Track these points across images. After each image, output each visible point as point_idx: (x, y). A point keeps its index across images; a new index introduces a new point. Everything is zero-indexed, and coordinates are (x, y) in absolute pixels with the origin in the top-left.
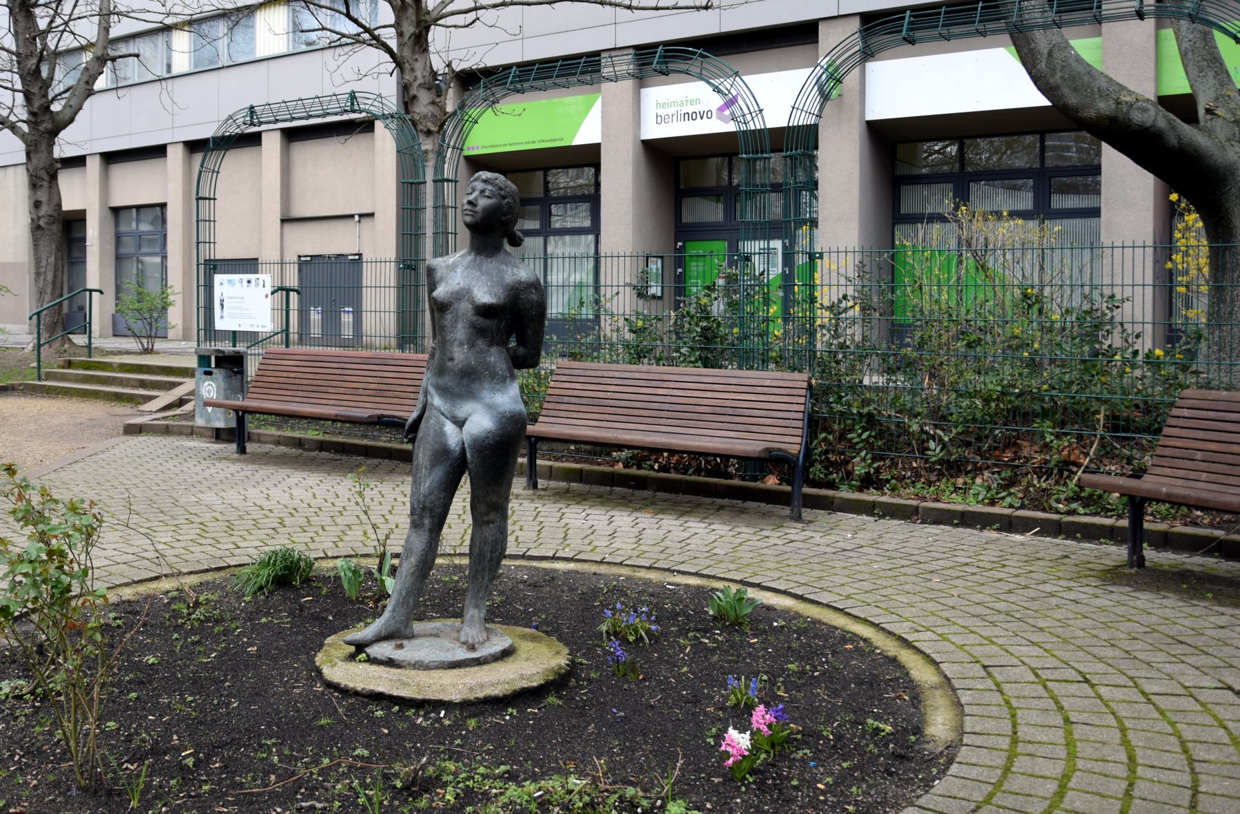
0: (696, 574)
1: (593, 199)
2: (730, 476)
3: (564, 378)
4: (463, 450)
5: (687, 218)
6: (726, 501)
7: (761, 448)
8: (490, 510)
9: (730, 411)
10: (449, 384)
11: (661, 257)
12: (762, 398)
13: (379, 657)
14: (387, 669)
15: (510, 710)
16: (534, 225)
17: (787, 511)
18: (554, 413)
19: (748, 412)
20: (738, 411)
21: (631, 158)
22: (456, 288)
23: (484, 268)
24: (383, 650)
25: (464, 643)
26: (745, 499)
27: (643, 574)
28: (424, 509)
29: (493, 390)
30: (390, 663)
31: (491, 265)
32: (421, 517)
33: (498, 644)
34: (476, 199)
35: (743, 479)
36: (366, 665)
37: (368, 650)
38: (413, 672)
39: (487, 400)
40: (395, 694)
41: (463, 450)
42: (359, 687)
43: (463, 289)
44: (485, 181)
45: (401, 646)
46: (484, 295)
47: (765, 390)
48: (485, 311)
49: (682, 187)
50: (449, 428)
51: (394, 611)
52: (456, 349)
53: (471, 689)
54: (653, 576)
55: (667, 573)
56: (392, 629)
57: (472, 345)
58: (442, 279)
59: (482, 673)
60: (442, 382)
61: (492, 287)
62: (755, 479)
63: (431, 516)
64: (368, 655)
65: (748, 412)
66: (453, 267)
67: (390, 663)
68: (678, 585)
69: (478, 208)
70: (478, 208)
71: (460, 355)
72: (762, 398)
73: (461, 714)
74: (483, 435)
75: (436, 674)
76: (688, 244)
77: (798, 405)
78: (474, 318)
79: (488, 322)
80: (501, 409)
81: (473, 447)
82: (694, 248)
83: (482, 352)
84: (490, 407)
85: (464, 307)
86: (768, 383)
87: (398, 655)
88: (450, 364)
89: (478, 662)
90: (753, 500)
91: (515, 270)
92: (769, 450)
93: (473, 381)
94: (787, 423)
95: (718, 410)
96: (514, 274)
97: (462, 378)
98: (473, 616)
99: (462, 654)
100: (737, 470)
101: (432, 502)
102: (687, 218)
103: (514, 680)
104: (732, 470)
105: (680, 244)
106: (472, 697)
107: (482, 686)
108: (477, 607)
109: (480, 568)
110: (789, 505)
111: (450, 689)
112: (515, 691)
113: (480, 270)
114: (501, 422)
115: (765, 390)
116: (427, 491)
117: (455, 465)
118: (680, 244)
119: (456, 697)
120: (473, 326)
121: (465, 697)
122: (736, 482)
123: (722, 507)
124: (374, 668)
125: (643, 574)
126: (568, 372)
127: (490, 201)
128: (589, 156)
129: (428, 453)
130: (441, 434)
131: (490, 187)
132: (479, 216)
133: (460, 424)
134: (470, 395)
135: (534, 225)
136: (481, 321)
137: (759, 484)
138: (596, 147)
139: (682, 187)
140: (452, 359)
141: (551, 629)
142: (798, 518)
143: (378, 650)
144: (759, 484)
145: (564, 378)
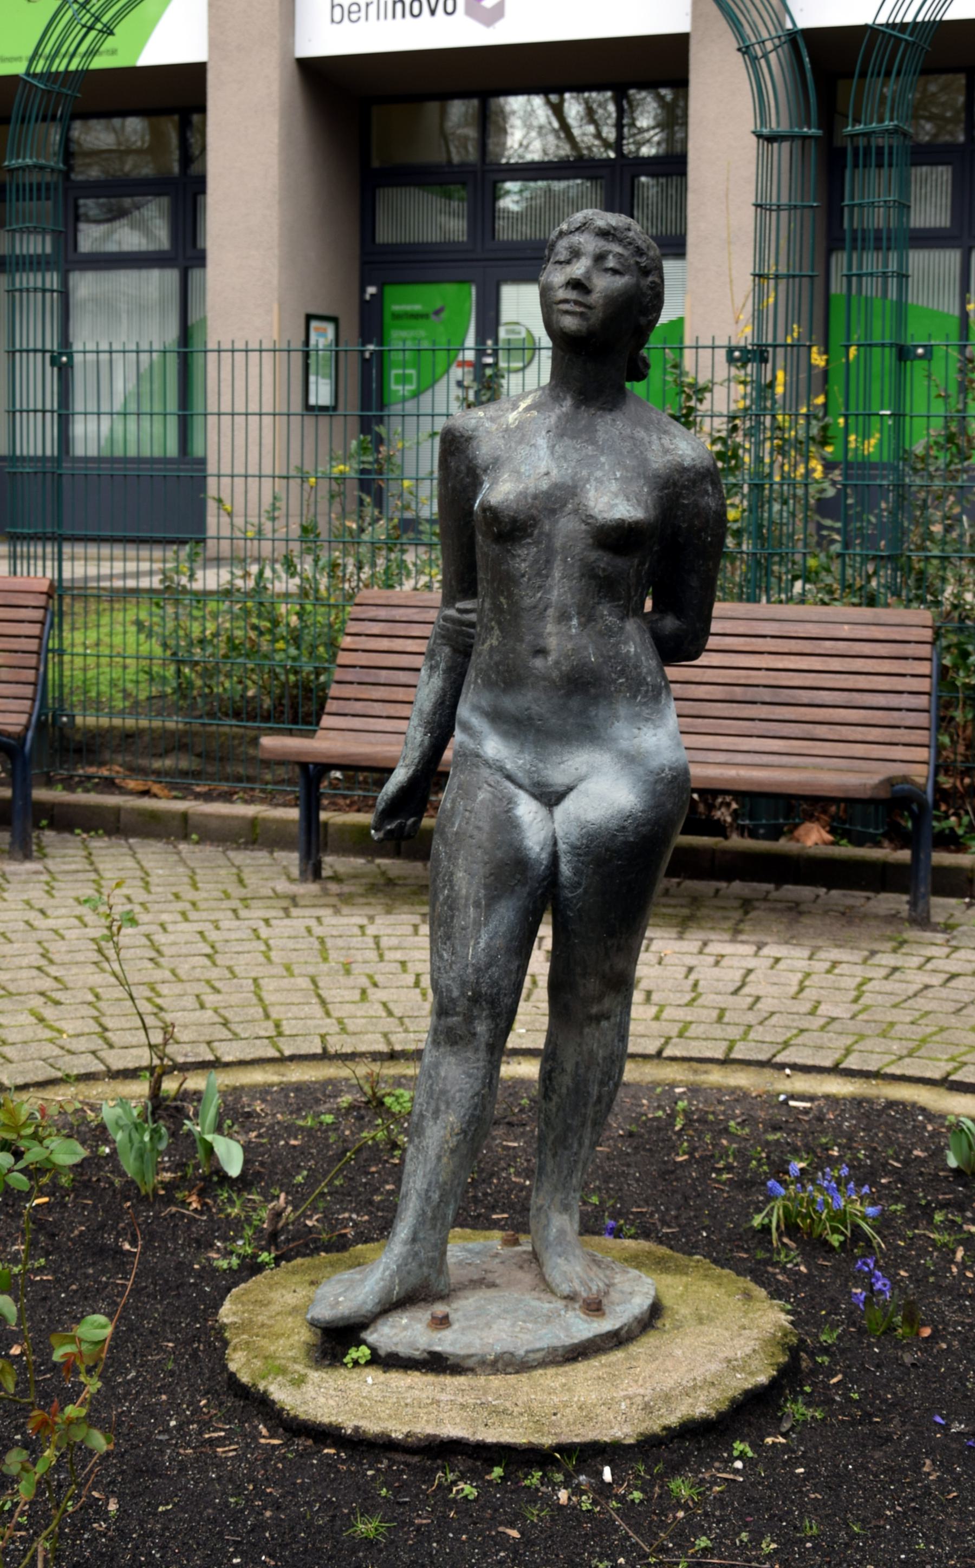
0: (836, 1070)
1: (184, 191)
2: (719, 829)
3: (376, 628)
4: (555, 857)
5: (385, 234)
6: (805, 892)
7: (875, 779)
8: (594, 985)
9: (767, 695)
10: (535, 708)
11: (334, 320)
12: (835, 664)
13: (403, 1351)
14: (430, 1378)
15: (739, 1446)
16: (37, 245)
17: (897, 902)
18: (358, 707)
19: (805, 696)
20: (785, 695)
21: (277, 106)
22: (544, 485)
23: (601, 436)
24: (405, 1332)
25: (571, 1298)
26: (780, 881)
27: (715, 1077)
28: (475, 1000)
29: (637, 719)
30: (435, 1363)
31: (611, 427)
32: (469, 1019)
33: (634, 1293)
34: (588, 274)
35: (753, 834)
36: (372, 1376)
37: (371, 1336)
38: (496, 1381)
39: (624, 744)
40: (490, 1439)
41: (555, 857)
42: (398, 1431)
43: (556, 486)
44: (605, 234)
45: (443, 1322)
46: (614, 501)
47: (842, 647)
48: (615, 538)
49: (376, 164)
50: (527, 809)
51: (414, 1239)
52: (550, 628)
53: (647, 1408)
54: (741, 1079)
55: (768, 1073)
56: (413, 1281)
57: (588, 617)
58: (496, 464)
59: (644, 1368)
60: (509, 703)
61: (625, 480)
62: (775, 833)
63: (473, 1011)
64: (374, 1350)
65: (805, 696)
66: (519, 434)
67: (435, 1363)
68: (811, 1098)
69: (595, 298)
70: (595, 298)
71: (560, 640)
72: (835, 664)
73: (649, 1470)
74: (613, 824)
75: (551, 1378)
76: (390, 291)
77: (918, 679)
78: (593, 555)
79: (620, 562)
80: (655, 763)
81: (575, 850)
82: (403, 300)
83: (609, 632)
84: (631, 759)
85: (566, 528)
86: (846, 631)
87: (447, 1342)
88: (538, 663)
89: (617, 1340)
90: (796, 883)
91: (666, 441)
92: (890, 782)
93: (595, 700)
94: (893, 718)
95: (738, 693)
96: (666, 451)
97: (569, 695)
98: (562, 1232)
99: (584, 1328)
100: (735, 814)
101: (494, 983)
102: (385, 234)
103: (719, 1375)
104: (723, 815)
105: (371, 290)
106: (655, 1426)
107: (667, 1398)
108: (566, 1208)
109: (575, 1122)
110: (903, 890)
111: (605, 1414)
112: (733, 1401)
113: (592, 441)
114: (653, 793)
115: (842, 647)
116: (483, 958)
117: (533, 888)
118: (371, 290)
119: (622, 1430)
120: (589, 573)
121: (642, 1428)
122: (737, 842)
123: (747, 905)
124: (399, 1380)
125: (715, 1077)
126: (382, 613)
127: (620, 282)
128: (178, 95)
129: (480, 870)
130: (507, 823)
131: (617, 248)
132: (596, 316)
133: (550, 797)
134: (587, 732)
135: (37, 245)
136: (603, 560)
137: (783, 845)
138: (193, 76)
139: (376, 164)
140: (541, 652)
141: (742, 1253)
142: (922, 921)
143: (405, 1332)
144: (783, 845)
145: (376, 628)
